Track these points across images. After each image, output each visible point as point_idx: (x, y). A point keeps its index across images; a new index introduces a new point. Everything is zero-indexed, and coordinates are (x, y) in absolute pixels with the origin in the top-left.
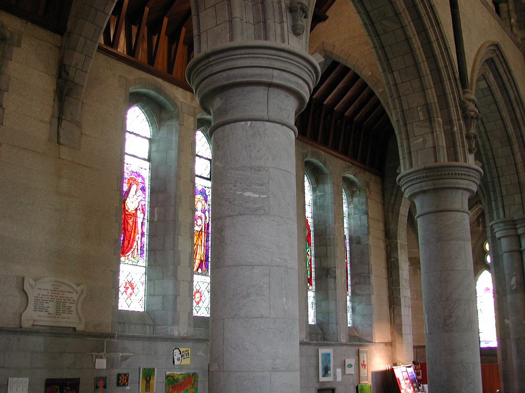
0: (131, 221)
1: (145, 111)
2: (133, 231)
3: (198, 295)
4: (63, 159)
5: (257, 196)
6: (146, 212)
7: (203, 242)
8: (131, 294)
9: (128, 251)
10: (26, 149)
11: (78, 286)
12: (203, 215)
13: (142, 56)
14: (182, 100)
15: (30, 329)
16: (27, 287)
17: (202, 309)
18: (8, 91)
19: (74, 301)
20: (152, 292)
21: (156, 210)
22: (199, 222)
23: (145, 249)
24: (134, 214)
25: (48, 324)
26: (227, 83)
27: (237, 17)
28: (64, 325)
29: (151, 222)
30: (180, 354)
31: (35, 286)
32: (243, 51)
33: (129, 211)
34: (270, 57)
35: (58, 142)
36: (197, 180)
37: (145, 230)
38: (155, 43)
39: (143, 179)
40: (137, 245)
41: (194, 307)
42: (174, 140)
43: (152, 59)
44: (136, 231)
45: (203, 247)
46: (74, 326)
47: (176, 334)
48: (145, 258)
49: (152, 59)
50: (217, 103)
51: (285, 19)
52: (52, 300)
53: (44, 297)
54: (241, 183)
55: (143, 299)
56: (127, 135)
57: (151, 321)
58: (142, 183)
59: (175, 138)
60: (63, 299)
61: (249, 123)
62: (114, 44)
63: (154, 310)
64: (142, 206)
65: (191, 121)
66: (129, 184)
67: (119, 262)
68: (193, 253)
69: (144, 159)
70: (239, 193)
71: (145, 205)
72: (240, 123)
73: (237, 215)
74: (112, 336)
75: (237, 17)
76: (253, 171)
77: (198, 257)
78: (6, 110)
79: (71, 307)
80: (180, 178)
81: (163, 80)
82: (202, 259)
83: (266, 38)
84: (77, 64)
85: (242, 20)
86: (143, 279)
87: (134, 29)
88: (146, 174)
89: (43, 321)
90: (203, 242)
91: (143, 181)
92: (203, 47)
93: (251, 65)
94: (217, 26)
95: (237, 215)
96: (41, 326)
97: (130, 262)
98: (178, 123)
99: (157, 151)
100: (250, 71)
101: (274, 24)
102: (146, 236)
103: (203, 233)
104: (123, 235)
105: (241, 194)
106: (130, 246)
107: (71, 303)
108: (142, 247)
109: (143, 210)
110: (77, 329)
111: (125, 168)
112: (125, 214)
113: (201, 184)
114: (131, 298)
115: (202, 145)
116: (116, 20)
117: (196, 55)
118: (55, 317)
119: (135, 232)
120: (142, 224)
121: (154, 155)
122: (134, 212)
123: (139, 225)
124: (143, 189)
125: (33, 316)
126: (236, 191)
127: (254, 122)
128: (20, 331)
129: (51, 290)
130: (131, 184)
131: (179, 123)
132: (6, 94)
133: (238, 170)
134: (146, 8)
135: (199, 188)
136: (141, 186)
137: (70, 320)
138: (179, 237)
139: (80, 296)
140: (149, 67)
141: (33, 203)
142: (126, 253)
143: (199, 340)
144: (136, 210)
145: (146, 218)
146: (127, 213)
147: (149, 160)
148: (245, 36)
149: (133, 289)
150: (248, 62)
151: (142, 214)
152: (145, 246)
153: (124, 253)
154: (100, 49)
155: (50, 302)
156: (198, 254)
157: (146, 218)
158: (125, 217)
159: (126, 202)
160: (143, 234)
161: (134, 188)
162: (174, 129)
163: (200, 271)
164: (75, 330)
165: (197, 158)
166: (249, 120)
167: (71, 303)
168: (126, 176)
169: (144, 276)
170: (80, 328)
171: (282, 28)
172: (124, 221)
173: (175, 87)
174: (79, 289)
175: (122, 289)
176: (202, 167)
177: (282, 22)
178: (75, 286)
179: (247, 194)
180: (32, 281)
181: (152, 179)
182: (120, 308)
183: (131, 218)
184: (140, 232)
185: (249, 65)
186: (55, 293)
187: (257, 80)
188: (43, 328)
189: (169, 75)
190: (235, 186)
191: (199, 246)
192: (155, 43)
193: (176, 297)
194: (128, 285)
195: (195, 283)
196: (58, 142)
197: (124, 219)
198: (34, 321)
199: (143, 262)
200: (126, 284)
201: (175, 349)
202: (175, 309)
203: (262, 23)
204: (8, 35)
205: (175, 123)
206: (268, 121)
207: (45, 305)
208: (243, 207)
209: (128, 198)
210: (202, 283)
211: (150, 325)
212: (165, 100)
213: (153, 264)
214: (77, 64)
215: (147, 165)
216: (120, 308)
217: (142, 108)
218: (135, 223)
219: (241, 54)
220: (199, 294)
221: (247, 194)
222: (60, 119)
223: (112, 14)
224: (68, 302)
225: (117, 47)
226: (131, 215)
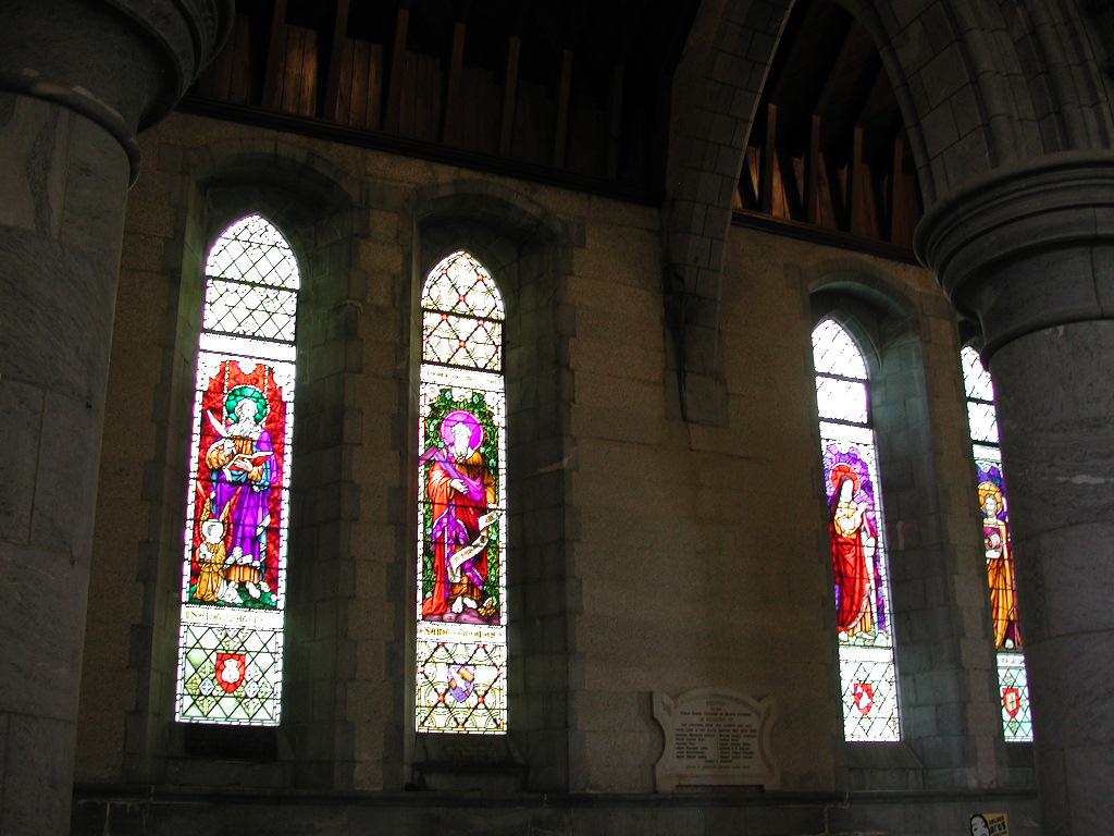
0: (850, 555)
1: (847, 325)
2: (858, 576)
3: (1011, 697)
4: (699, 450)
5: (1101, 480)
6: (880, 533)
7: (1008, 582)
8: (869, 708)
9: (853, 619)
10: (624, 442)
11: (759, 700)
12: (1000, 522)
13: (822, 214)
14: (919, 290)
15: (672, 794)
16: (659, 712)
17: (1019, 728)
18: (575, 336)
19: (754, 731)
20: (913, 700)
21: (899, 526)
22: (995, 539)
23: (886, 611)
24: (854, 540)
25: (705, 782)
26: (1002, 253)
27: (1000, 115)
28: (739, 781)
29: (891, 552)
30: (986, 825)
31: (675, 707)
32: (1024, 183)
33: (844, 535)
34: (1083, 182)
35: (685, 419)
36: (978, 451)
37: (882, 572)
38: (844, 184)
39: (864, 466)
40: (869, 604)
41: (1005, 725)
42: (916, 375)
43: (843, 216)
44: (865, 576)
45: (1009, 593)
46: (761, 783)
47: (973, 783)
48: (889, 628)
49: (843, 216)
50: (988, 298)
51: (1101, 95)
52: (711, 733)
53: (694, 728)
54: (1062, 459)
55: (896, 715)
56: (819, 380)
57: (917, 761)
58: (863, 474)
59: (917, 371)
60: (731, 729)
61: (1061, 329)
62: (764, 202)
63: (920, 737)
64: (869, 521)
65: (945, 329)
66: (837, 481)
67: (836, 644)
68: (990, 609)
69: (861, 425)
70: (1061, 479)
71: (875, 518)
72: (1043, 331)
73: (1064, 527)
74: (837, 798)
75: (1000, 115)
76: (1085, 430)
77: (1002, 615)
78: (576, 373)
79: (748, 744)
80: (942, 454)
81: (875, 256)
82: (1012, 618)
83: (1069, 146)
84: (697, 259)
85: (1010, 117)
86: (891, 673)
87: (799, 165)
88: (868, 455)
89: (697, 776)
90: (1008, 582)
91: (863, 471)
92: (945, 187)
93: (1046, 207)
94: (960, 139)
95: (1064, 527)
96: (695, 786)
97: (860, 642)
98: (918, 338)
99: (884, 404)
100: (1045, 220)
101: (1079, 110)
102: (885, 583)
103: (1007, 563)
104: (837, 587)
105: (1066, 482)
106: (855, 608)
107: (749, 736)
108: (880, 608)
109: (872, 529)
110: (765, 788)
111: (824, 448)
112: (838, 543)
113: (987, 458)
114: (869, 715)
115: (977, 379)
116: (758, 153)
117: (930, 208)
118: (721, 767)
119: (862, 578)
120: (875, 558)
121: (878, 414)
122: (854, 536)
123: (869, 563)
124: (867, 487)
125: (676, 769)
126: (1056, 475)
127: (1072, 325)
128: (654, 799)
129: (706, 714)
130: (841, 480)
131: (921, 339)
132: (572, 342)
133: (1052, 430)
134: (814, 117)
135: (985, 468)
136: (861, 479)
137: (750, 771)
138: (956, 578)
139: (764, 723)
140: (841, 234)
141: (651, 546)
142: (850, 624)
143: (1027, 795)
144: (858, 531)
145: (880, 545)
146: (840, 540)
147: (870, 425)
148: (1023, 150)
149: (871, 695)
150: (1038, 204)
151: (872, 540)
152: (886, 603)
153: (844, 624)
154: (738, 220)
155: (708, 738)
156: (1000, 610)
157: (880, 545)
158: (838, 550)
159: (836, 518)
160: (878, 581)
161: (848, 486)
162: (914, 354)
163: (1009, 643)
164: (763, 791)
165: (969, 404)
166: (1059, 324)
167: (749, 736)
168: (827, 463)
169: (892, 666)
170: (772, 785)
171: (1100, 117)
172: (837, 558)
173: (901, 266)
174: (761, 706)
175: (848, 699)
176: (983, 423)
177: (1096, 104)
178: (752, 702)
179: (1079, 479)
180: (667, 699)
181: (882, 463)
182: (848, 739)
183: (850, 549)
184: (872, 577)
185: (1041, 209)
186: (715, 720)
187: (1063, 235)
188: (699, 790)
189: (885, 244)
190: (1050, 466)
191: (1001, 592)
192: (844, 184)
193: (963, 705)
194: (860, 690)
195: (1001, 673)
196: (685, 419)
197: (835, 555)
198: (681, 777)
199: (885, 639)
200: (856, 689)
201: (974, 816)
202: (964, 731)
203: (1053, 116)
204: (559, 229)
205: (912, 340)
206: (1103, 317)
207: (699, 744)
208: (1074, 507)
209: (838, 510)
210: (1012, 668)
211: (915, 769)
212: (885, 297)
213: (908, 639)
214: (697, 259)
215: (867, 435)
216: (848, 739)
217: (839, 320)
218: (860, 559)
219: (1018, 190)
220: (1013, 694)
221: (1079, 479)
222: (681, 373)
223: (749, 144)
224: (742, 735)
225: (770, 207)
226: (850, 544)
